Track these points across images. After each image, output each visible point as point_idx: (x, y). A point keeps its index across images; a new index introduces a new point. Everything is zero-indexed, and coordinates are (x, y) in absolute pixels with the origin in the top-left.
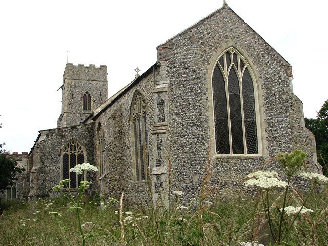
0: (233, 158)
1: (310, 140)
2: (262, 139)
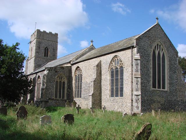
0: (158, 90)
1: (184, 85)
2: (167, 83)
